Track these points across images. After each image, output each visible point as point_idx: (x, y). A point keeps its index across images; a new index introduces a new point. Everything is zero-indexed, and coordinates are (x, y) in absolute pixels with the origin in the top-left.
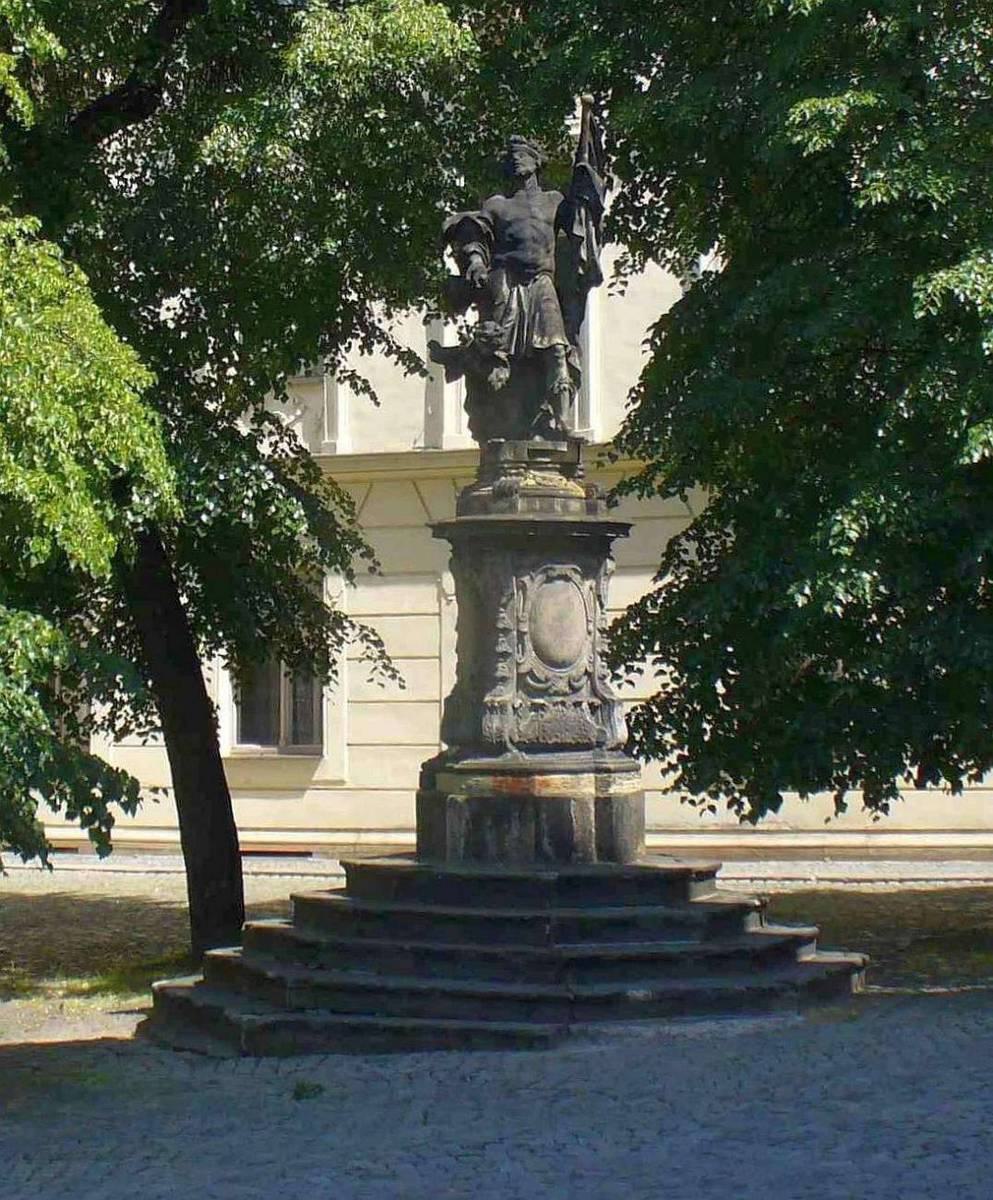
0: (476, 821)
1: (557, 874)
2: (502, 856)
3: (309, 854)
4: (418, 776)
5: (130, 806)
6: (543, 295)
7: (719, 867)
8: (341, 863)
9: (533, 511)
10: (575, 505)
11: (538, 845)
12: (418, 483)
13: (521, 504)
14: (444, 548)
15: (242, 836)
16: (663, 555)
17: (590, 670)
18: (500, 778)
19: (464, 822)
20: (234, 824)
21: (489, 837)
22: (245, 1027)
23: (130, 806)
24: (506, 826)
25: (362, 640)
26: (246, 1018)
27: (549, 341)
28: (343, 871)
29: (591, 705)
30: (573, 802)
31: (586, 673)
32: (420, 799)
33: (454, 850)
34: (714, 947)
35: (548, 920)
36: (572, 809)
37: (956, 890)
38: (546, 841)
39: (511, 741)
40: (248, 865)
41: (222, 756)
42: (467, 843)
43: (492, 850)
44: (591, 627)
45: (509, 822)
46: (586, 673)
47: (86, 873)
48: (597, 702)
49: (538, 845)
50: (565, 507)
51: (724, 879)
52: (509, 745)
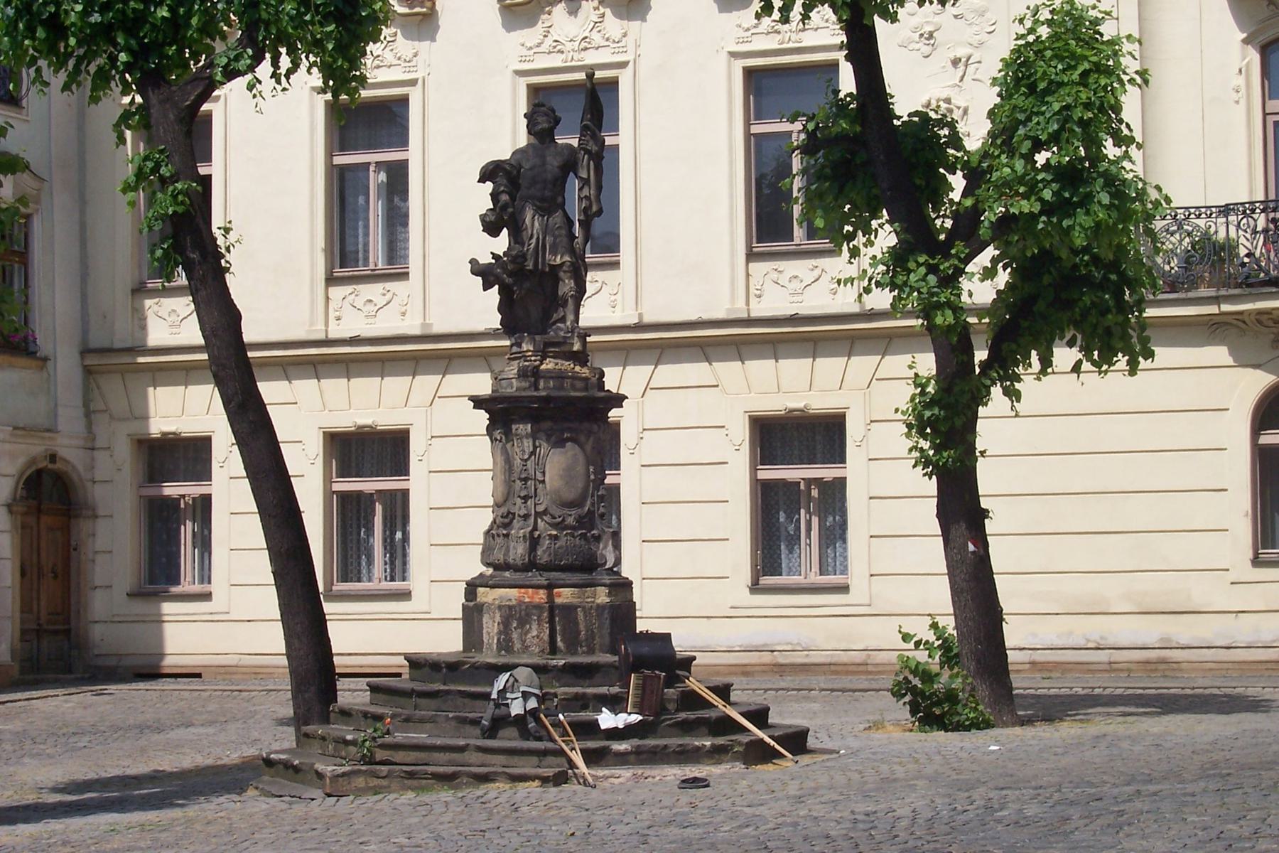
0: (506, 623)
1: (564, 662)
2: (525, 648)
4: (464, 591)
5: (870, 263)
8: (405, 659)
14: (482, 417)
15: (336, 660)
18: (523, 590)
19: (496, 624)
21: (515, 635)
22: (328, 774)
23: (870, 263)
24: (528, 626)
25: (814, 115)
26: (330, 768)
28: (406, 663)
33: (490, 645)
35: (556, 695)
37: (1155, 695)
41: (933, 354)
42: (498, 640)
43: (517, 646)
45: (530, 624)
47: (208, 693)
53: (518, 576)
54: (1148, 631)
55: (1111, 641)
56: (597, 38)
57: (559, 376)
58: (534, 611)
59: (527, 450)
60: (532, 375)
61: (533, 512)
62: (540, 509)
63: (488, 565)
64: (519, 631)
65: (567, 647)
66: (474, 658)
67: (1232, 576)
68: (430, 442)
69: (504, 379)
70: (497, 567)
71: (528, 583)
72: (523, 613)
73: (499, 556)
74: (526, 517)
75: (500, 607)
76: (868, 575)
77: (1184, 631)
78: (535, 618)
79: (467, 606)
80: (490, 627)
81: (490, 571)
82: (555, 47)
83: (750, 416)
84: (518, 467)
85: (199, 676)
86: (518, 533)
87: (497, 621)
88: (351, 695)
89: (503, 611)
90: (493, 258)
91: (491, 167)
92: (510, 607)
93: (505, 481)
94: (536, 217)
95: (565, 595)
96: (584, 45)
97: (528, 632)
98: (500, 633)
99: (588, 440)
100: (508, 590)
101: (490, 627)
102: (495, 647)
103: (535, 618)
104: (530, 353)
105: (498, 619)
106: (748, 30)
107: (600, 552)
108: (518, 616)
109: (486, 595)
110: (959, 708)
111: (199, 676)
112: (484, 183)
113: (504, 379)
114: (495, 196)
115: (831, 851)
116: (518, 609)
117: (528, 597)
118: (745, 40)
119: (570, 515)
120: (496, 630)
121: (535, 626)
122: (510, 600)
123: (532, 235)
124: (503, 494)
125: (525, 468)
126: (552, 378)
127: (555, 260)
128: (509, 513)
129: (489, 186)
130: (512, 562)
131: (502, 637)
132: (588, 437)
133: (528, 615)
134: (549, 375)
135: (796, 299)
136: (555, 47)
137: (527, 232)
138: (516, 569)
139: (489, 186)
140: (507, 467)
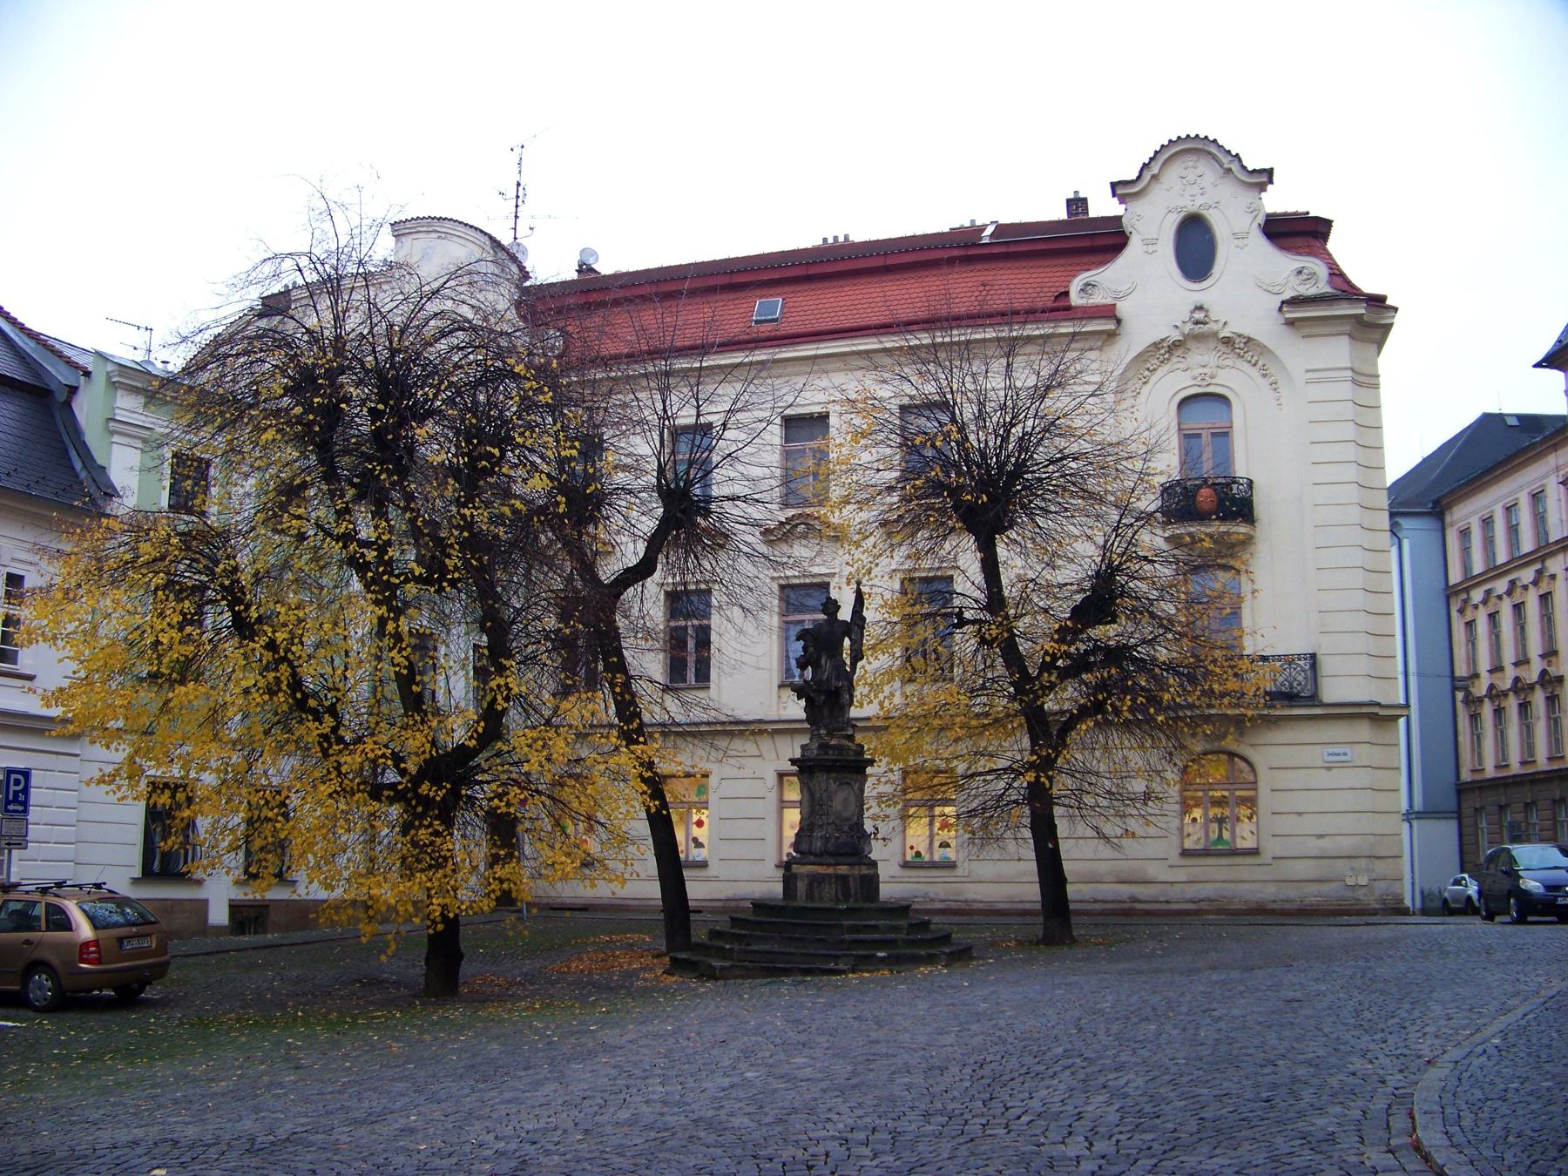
0: (811, 884)
2: (821, 899)
15: (690, 903)
21: (816, 893)
34: (911, 937)
38: (840, 894)
53: (817, 860)
54: (1125, 890)
55: (1100, 898)
57: (839, 748)
60: (824, 747)
67: (1170, 862)
73: (804, 847)
74: (821, 826)
77: (1141, 891)
80: (801, 886)
85: (700, 912)
88: (699, 934)
95: (843, 870)
101: (801, 886)
109: (796, 868)
110: (405, 851)
111: (700, 912)
114: (805, 648)
115: (1230, 1171)
129: (802, 643)
134: (834, 747)
138: (816, 855)
139: (802, 643)
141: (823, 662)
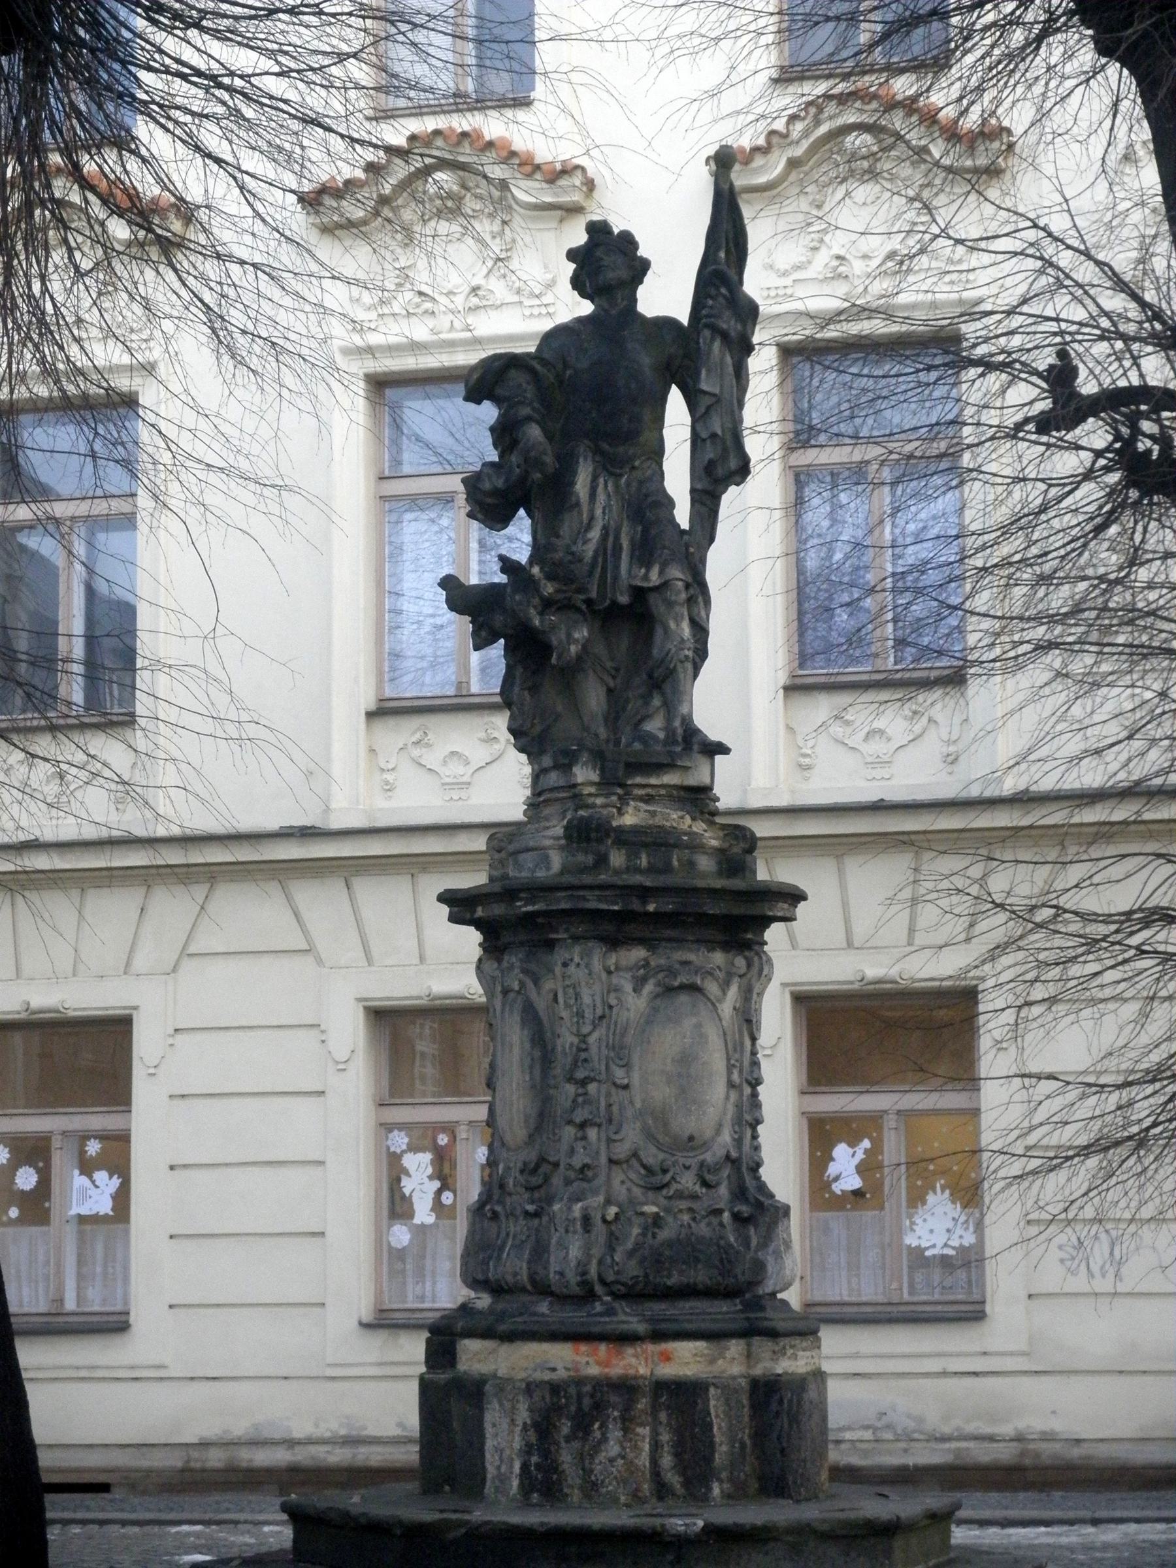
2: (591, 1488)
3: (104, 1488)
6: (647, 496)
7: (958, 1506)
8: (285, 1508)
9: (638, 870)
10: (705, 863)
11: (656, 1472)
12: (192, 949)
13: (617, 859)
16: (111, 1178)
17: (734, 1154)
20: (32, 1440)
21: (566, 1457)
27: (661, 573)
29: (736, 1217)
30: (712, 1391)
31: (728, 1157)
32: (426, 1388)
36: (712, 1403)
39: (602, 1281)
40: (55, 1507)
42: (525, 1467)
44: (735, 1077)
46: (728, 1157)
48: (745, 1209)
49: (656, 1472)
50: (692, 864)
51: (66, 1523)
52: (599, 1289)
56: (498, 289)
58: (614, 1398)
59: (588, 1014)
61: (603, 1160)
62: (622, 1150)
63: (474, 1283)
64: (576, 1444)
65: (687, 1483)
66: (469, 1512)
68: (171, 1041)
69: (528, 850)
70: (497, 1289)
71: (596, 1329)
72: (587, 1402)
75: (530, 1388)
76: (1023, 1294)
78: (616, 1414)
79: (432, 1382)
81: (484, 1301)
82: (418, 306)
83: (792, 993)
84: (564, 1053)
86: (569, 1209)
87: (520, 1422)
89: (537, 1396)
90: (503, 570)
91: (475, 377)
92: (555, 1388)
93: (533, 1087)
94: (601, 480)
96: (474, 301)
97: (597, 1448)
98: (528, 1450)
99: (725, 993)
100: (546, 1346)
102: (515, 1483)
103: (616, 1414)
104: (592, 790)
105: (523, 1415)
106: (785, 274)
107: (752, 1254)
108: (573, 1408)
112: (479, 402)
113: (528, 850)
116: (572, 1390)
117: (598, 1363)
118: (781, 292)
119: (687, 1168)
120: (517, 1444)
121: (615, 1433)
122: (554, 1370)
123: (592, 518)
124: (527, 1118)
125: (583, 1055)
126: (646, 845)
127: (646, 578)
128: (542, 1160)
130: (509, 1278)
131: (534, 1459)
132: (725, 985)
133: (599, 1407)
134: (630, 839)
135: (878, 773)
136: (418, 306)
137: (580, 513)
140: (537, 1054)
141: (581, 486)
